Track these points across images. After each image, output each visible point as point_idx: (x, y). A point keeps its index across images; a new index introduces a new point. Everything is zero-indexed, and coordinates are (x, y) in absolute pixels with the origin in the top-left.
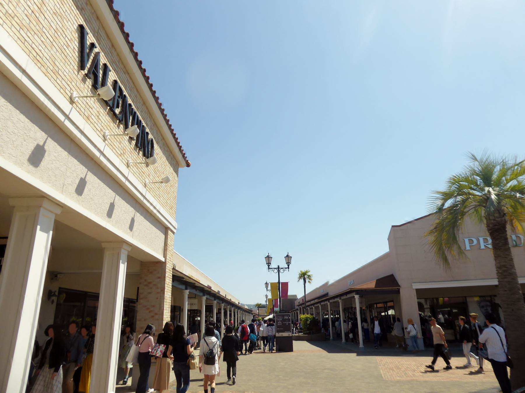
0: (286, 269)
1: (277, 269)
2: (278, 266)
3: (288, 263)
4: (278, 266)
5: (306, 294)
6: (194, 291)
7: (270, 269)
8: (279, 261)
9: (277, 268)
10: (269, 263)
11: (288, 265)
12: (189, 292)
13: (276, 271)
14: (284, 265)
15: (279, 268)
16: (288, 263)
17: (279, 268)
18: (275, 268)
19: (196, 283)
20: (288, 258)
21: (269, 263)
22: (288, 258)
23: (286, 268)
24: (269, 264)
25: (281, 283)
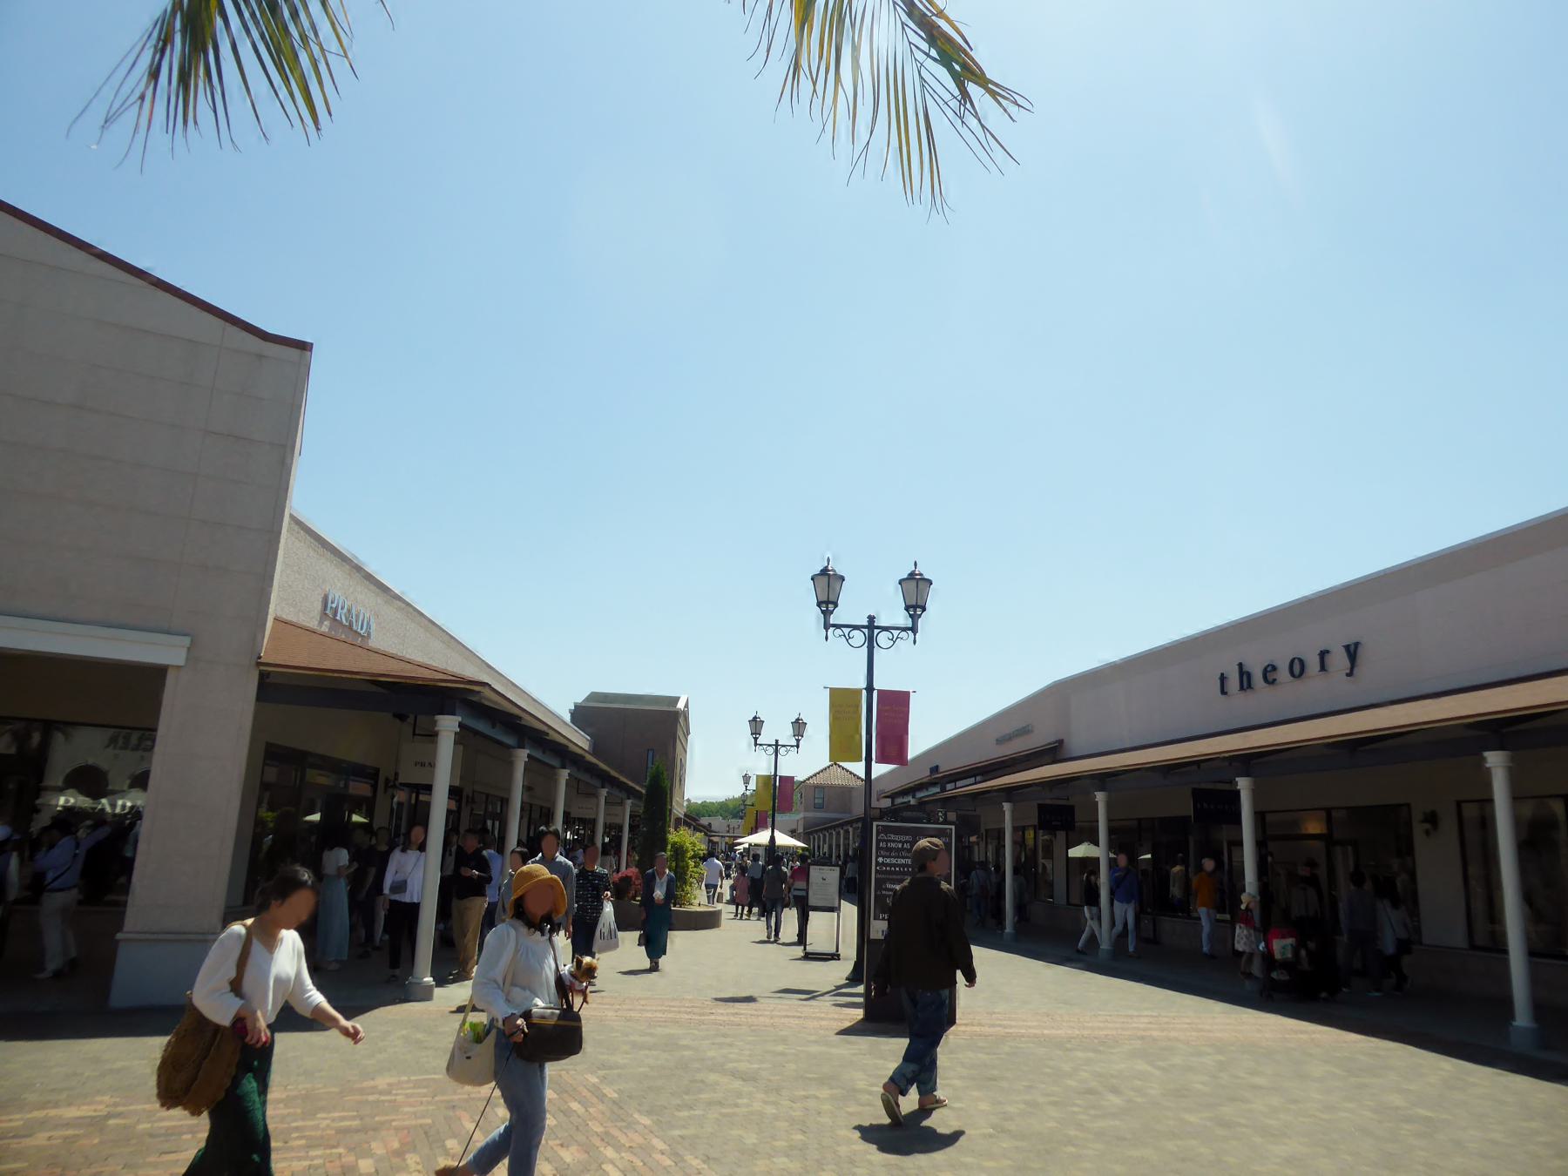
0: (903, 634)
1: (866, 631)
2: (871, 619)
3: (915, 608)
4: (871, 619)
5: (873, 777)
6: (616, 792)
7: (831, 629)
8: (777, 729)
9: (864, 627)
10: (827, 603)
11: (914, 618)
12: (529, 756)
13: (859, 637)
14: (786, 737)
15: (777, 744)
16: (915, 608)
17: (777, 744)
18: (769, 745)
19: (551, 732)
20: (916, 591)
21: (827, 603)
22: (916, 591)
23: (792, 746)
24: (827, 604)
25: (880, 692)
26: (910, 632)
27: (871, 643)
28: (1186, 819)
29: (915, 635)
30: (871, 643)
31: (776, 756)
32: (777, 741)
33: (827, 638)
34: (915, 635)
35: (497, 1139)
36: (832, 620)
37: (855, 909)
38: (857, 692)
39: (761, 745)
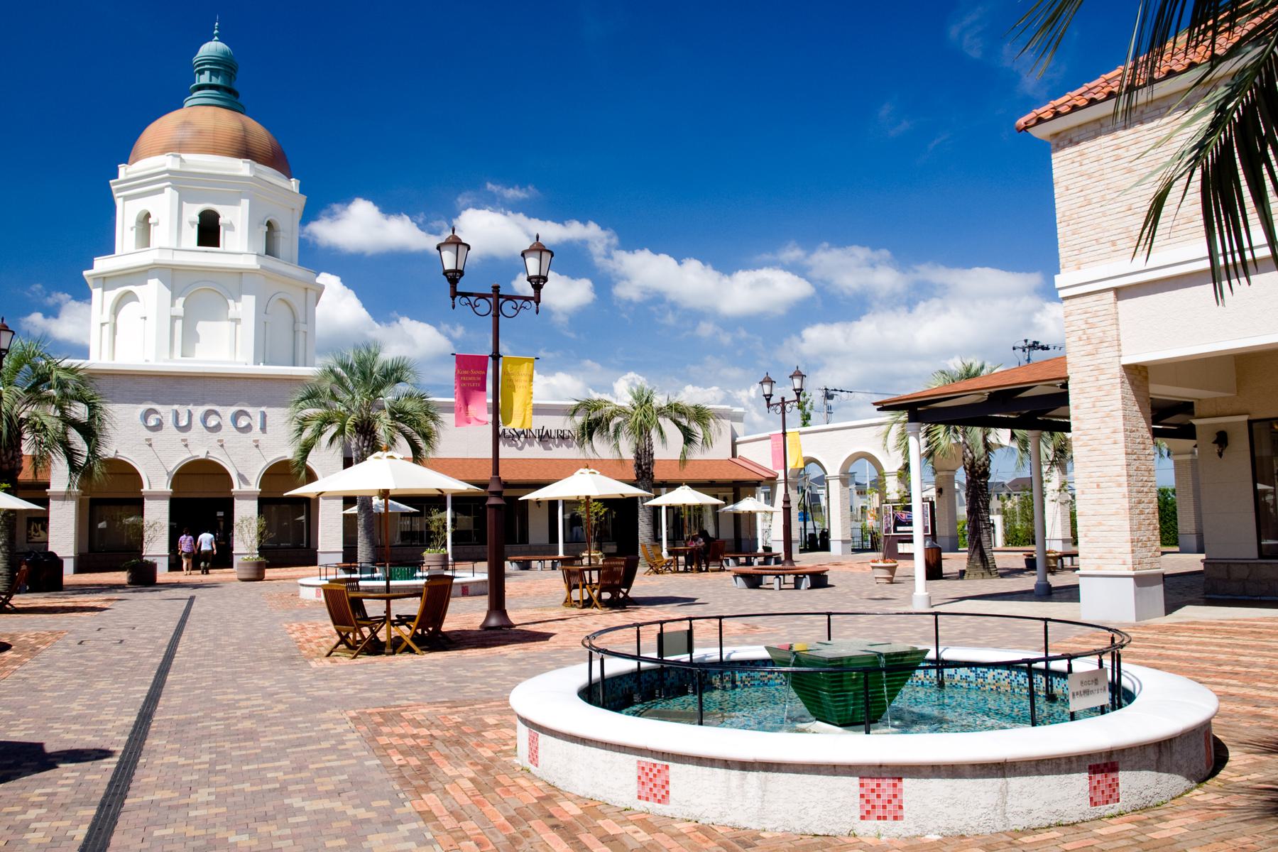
0: (526, 304)
7: (458, 297)
9: (490, 296)
13: (484, 306)
26: (533, 302)
27: (497, 312)
28: (469, 532)
29: (537, 305)
30: (497, 312)
31: (496, 317)
32: (496, 288)
33: (454, 307)
34: (537, 305)
35: (517, 187)
36: (460, 288)
37: (1032, 587)
38: (485, 359)
39: (465, 295)
